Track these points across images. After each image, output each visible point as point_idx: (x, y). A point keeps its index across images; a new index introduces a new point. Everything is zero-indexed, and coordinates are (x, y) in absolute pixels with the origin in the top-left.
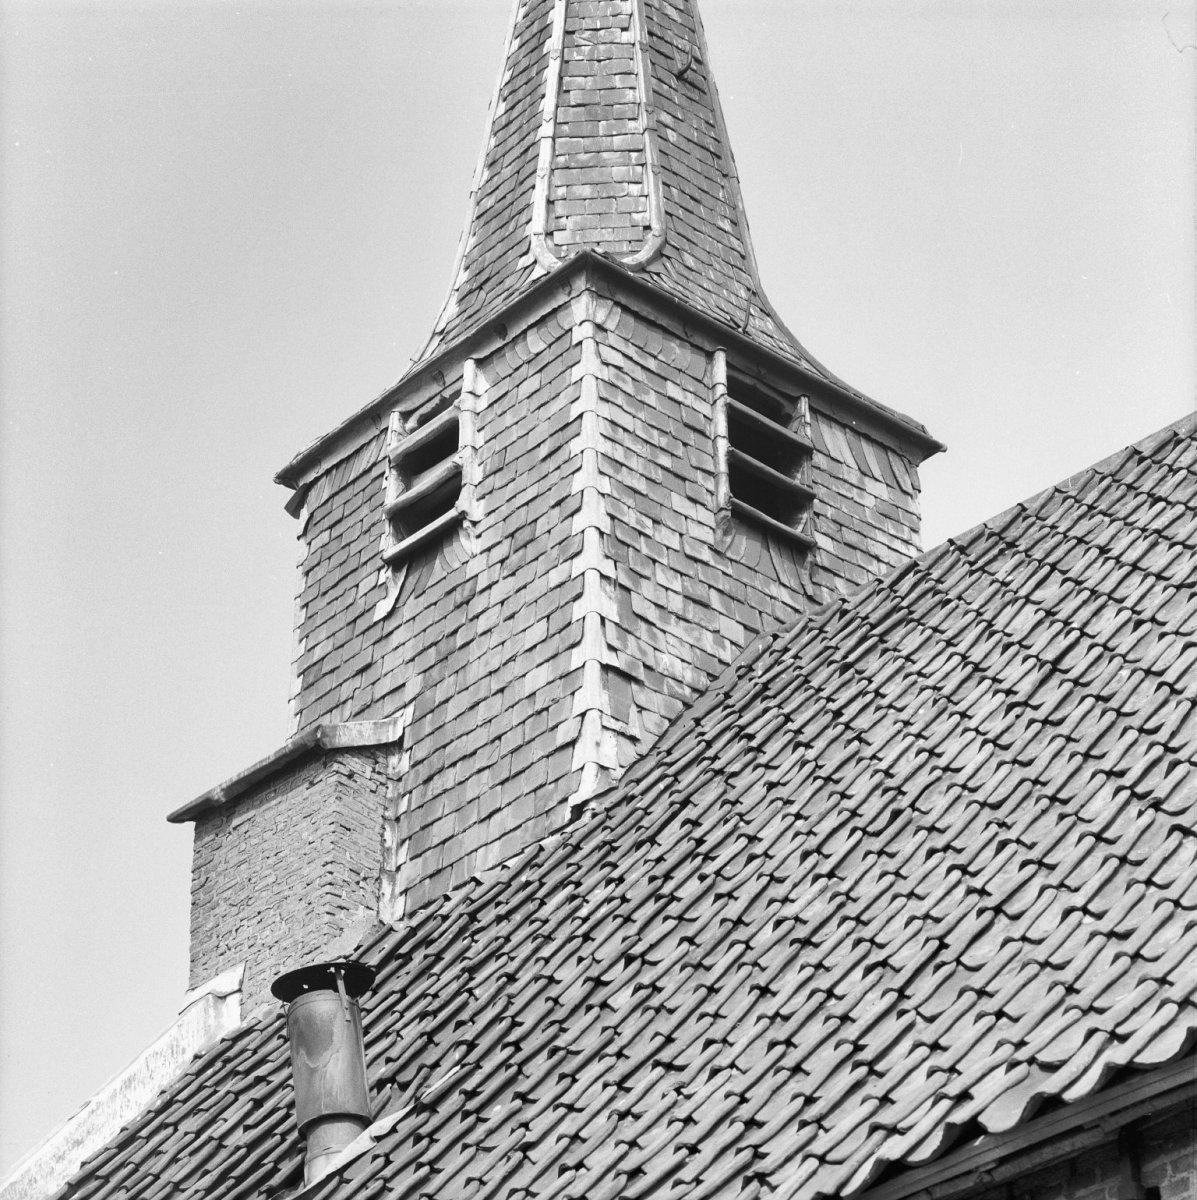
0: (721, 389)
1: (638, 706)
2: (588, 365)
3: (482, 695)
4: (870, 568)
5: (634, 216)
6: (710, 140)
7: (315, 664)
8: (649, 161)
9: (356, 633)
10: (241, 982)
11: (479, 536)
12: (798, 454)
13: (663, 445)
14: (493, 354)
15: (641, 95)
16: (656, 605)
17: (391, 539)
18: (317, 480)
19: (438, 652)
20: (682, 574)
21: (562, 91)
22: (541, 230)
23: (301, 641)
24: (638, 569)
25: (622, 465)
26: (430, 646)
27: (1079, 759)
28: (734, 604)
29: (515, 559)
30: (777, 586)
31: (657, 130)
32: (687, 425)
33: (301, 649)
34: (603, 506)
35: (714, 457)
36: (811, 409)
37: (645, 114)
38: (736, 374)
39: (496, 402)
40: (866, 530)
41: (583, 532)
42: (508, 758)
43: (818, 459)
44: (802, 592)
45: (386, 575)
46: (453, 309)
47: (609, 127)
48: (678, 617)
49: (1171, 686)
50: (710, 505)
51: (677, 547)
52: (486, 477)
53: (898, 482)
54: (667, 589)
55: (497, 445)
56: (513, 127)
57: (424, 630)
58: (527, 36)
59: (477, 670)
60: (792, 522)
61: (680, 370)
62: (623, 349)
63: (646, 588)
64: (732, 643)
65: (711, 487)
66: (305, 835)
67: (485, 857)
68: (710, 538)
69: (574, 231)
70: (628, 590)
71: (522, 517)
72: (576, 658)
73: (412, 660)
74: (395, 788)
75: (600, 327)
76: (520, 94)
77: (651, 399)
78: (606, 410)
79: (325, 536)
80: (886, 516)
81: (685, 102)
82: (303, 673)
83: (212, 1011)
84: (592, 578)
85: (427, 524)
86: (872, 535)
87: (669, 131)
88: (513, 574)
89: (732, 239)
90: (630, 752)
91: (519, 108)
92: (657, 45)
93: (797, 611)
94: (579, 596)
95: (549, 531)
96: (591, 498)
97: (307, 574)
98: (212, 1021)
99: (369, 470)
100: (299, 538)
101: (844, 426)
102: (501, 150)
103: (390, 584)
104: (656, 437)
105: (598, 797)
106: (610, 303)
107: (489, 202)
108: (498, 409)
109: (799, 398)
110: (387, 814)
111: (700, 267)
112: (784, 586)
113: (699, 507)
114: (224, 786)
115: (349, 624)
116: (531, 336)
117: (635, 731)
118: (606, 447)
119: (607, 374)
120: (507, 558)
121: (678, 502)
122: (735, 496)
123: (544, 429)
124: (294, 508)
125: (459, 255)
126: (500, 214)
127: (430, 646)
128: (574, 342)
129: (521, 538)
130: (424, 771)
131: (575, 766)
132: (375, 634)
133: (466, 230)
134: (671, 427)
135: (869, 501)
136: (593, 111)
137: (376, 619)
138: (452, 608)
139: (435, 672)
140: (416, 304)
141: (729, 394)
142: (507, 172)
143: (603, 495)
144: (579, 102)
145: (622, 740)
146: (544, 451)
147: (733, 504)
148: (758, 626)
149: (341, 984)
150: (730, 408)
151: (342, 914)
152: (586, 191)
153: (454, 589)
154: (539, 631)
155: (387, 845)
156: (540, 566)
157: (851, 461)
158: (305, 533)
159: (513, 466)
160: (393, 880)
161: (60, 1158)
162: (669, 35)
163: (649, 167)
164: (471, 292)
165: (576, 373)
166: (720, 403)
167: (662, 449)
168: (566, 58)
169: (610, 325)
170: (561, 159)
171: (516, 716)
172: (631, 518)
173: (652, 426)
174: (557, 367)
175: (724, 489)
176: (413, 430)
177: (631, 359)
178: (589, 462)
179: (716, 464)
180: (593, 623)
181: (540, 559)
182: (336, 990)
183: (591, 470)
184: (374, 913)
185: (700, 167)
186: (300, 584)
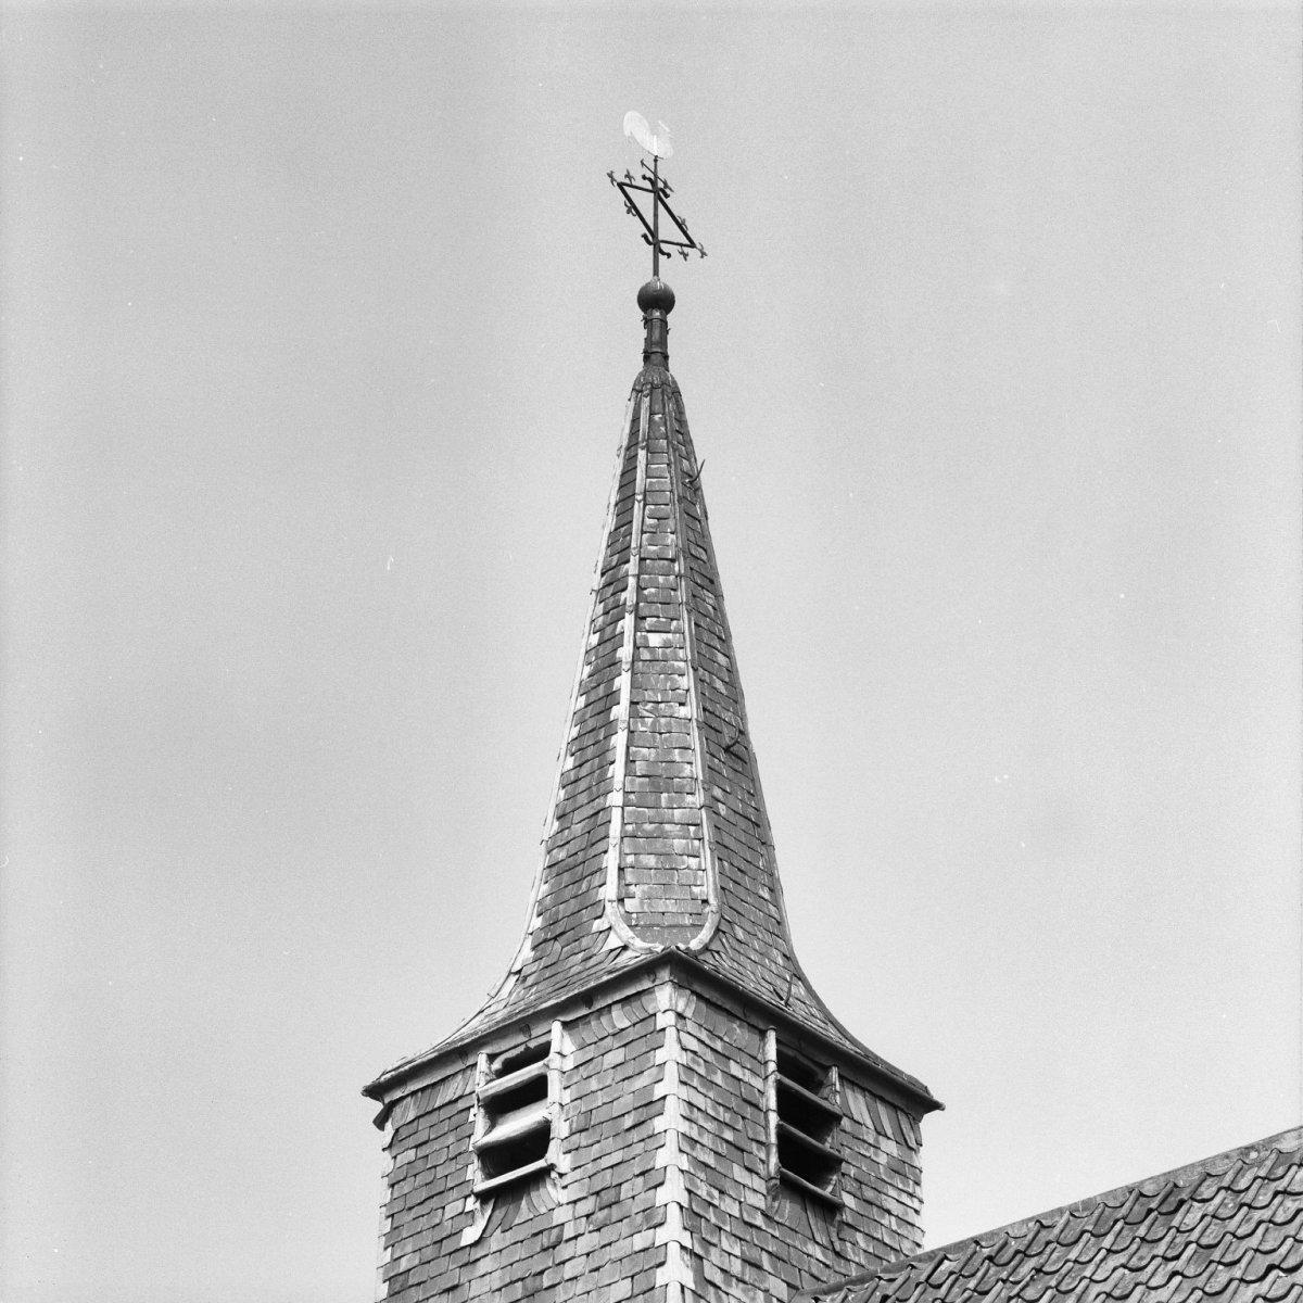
0: (772, 1066)
2: (669, 1053)
4: (883, 1222)
5: (693, 888)
6: (751, 810)
7: (401, 1274)
8: (706, 838)
11: (565, 1187)
12: (826, 1121)
13: (727, 1121)
14: (577, 1019)
15: (697, 770)
16: (722, 1270)
17: (479, 1175)
18: (402, 1098)
19: (525, 1288)
20: (741, 1239)
22: (614, 898)
23: (386, 1249)
24: (708, 1238)
25: (697, 1142)
28: (779, 1264)
29: (600, 1215)
31: (710, 806)
32: (745, 1100)
33: (387, 1256)
35: (766, 1127)
36: (841, 1077)
37: (702, 790)
39: (581, 1065)
40: (879, 1185)
41: (666, 1205)
43: (845, 1122)
44: (831, 1248)
45: (471, 1204)
46: (527, 953)
47: (670, 800)
48: (738, 1279)
50: (763, 1173)
51: (737, 1215)
52: (572, 1134)
53: (905, 1139)
54: (730, 1254)
57: (512, 1265)
60: (823, 1183)
61: (740, 1049)
62: (698, 1035)
65: (763, 1156)
68: (760, 1202)
70: (701, 1258)
71: (607, 1178)
73: (500, 1289)
75: (680, 1016)
77: (718, 1079)
78: (684, 1092)
80: (895, 1172)
82: (389, 1279)
84: (674, 1249)
86: (885, 1191)
87: (720, 805)
89: (771, 907)
92: (709, 726)
93: (827, 1266)
94: (662, 1264)
95: (633, 1197)
96: (672, 1174)
97: (392, 1186)
99: (456, 1100)
100: (384, 1150)
101: (863, 1090)
103: (478, 1214)
106: (688, 992)
107: (561, 854)
109: (830, 1067)
112: (817, 1243)
113: (754, 1176)
115: (435, 1243)
116: (616, 1012)
118: (684, 1127)
119: (685, 1058)
120: (593, 1214)
121: (739, 1173)
122: (783, 1167)
123: (627, 1101)
124: (380, 1122)
125: (532, 901)
129: (607, 1199)
132: (463, 1258)
133: (538, 877)
134: (734, 1103)
135: (883, 1159)
136: (657, 782)
137: (463, 1244)
138: (538, 1249)
141: (778, 1071)
142: (578, 829)
143: (682, 1171)
144: (644, 773)
146: (628, 1121)
147: (781, 1173)
148: (798, 1284)
150: (779, 1084)
152: (651, 861)
153: (541, 1232)
156: (624, 1228)
157: (869, 1123)
158: (390, 1146)
163: (706, 843)
164: (545, 941)
166: (772, 1079)
167: (726, 1124)
168: (632, 729)
169: (689, 1014)
170: (629, 828)
173: (720, 1104)
174: (640, 1047)
175: (774, 1159)
178: (671, 1140)
179: (767, 1135)
181: (625, 1221)
183: (673, 1149)
185: (744, 840)
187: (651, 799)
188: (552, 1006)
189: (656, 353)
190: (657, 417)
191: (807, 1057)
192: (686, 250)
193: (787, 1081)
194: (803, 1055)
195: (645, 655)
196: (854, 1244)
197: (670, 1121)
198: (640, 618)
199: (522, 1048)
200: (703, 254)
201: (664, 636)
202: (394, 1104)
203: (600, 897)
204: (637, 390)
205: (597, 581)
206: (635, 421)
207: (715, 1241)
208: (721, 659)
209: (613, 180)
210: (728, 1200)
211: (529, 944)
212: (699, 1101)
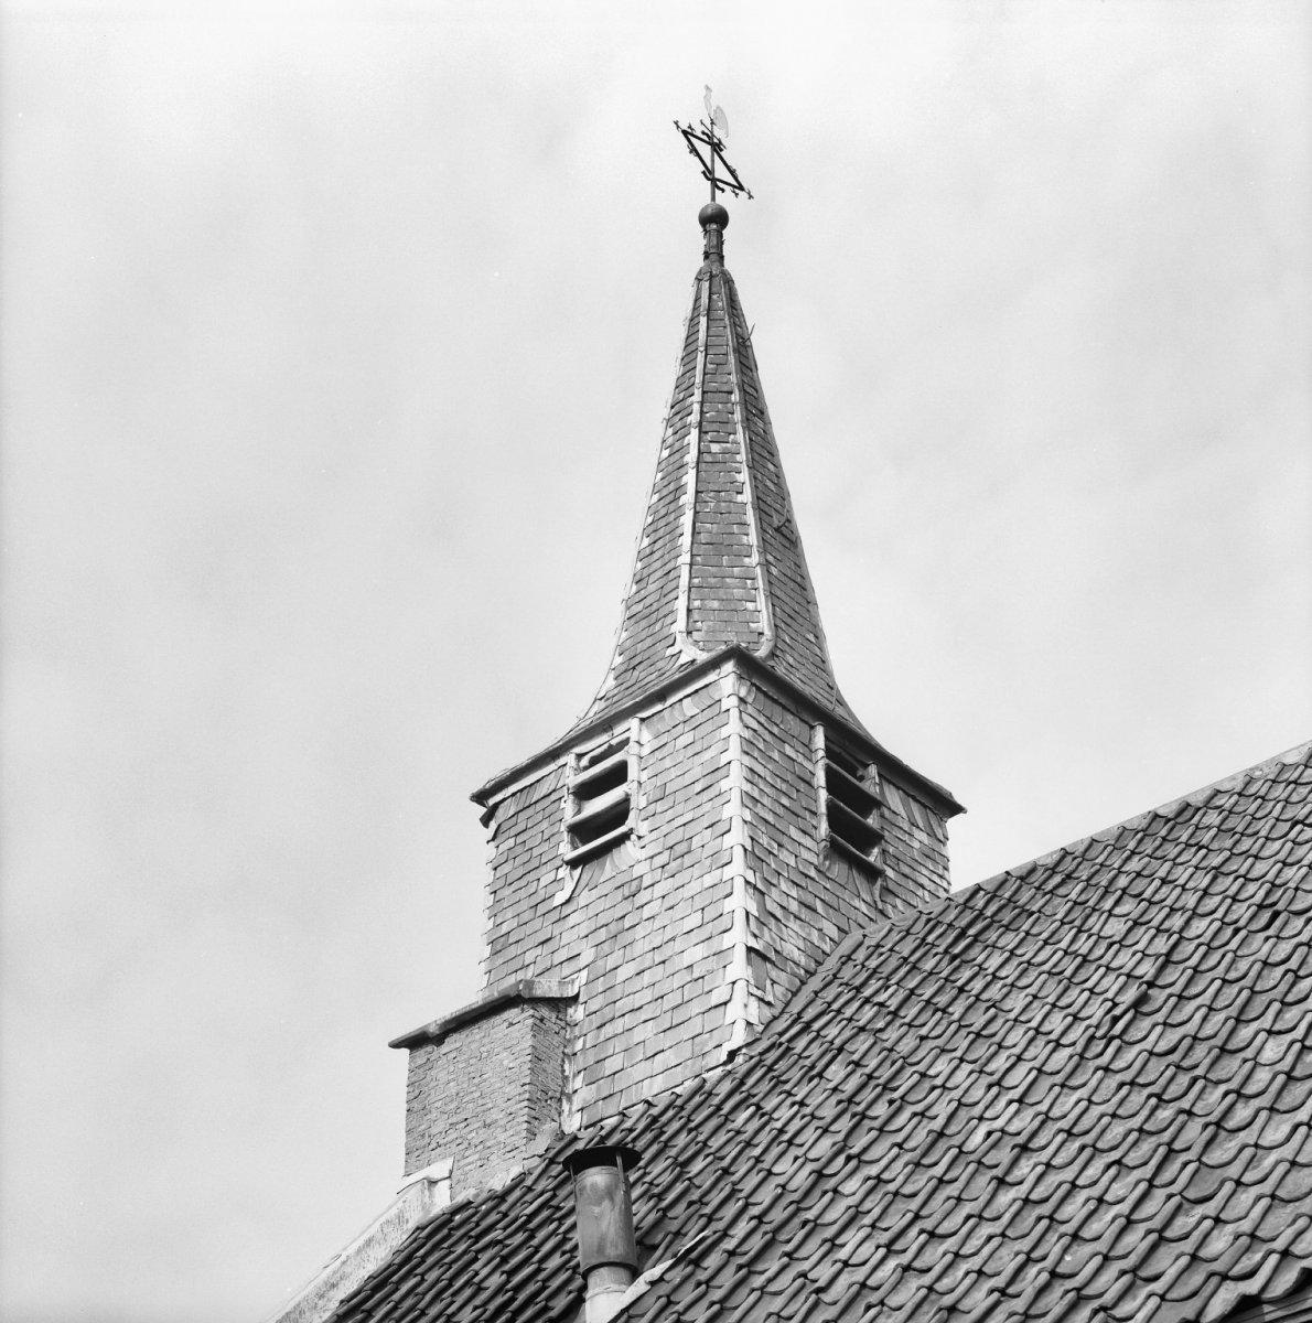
0: (821, 753)
1: (772, 980)
3: (647, 965)
5: (751, 625)
9: (538, 915)
10: (451, 1172)
12: (870, 804)
20: (798, 885)
21: (694, 532)
25: (757, 801)
26: (602, 927)
27: (879, 1089)
28: (831, 911)
30: (860, 896)
31: (766, 565)
33: (490, 924)
34: (747, 830)
38: (832, 746)
42: (669, 1014)
45: (564, 872)
46: (611, 683)
48: (796, 917)
49: (1295, 972)
55: (659, 781)
56: (656, 556)
58: (665, 492)
59: (639, 948)
63: (774, 893)
64: (830, 939)
66: (505, 1062)
67: (651, 1087)
69: (707, 632)
70: (763, 894)
71: (678, 835)
72: (726, 941)
74: (572, 1032)
76: (661, 533)
77: (776, 755)
78: (747, 760)
79: (511, 842)
81: (781, 548)
83: (426, 1192)
85: (599, 835)
88: (673, 876)
90: (768, 1013)
91: (660, 543)
93: (871, 919)
97: (495, 869)
98: (427, 1200)
99: (550, 794)
100: (488, 842)
101: (898, 788)
102: (646, 572)
104: (779, 784)
105: (748, 1045)
108: (658, 755)
110: (566, 1051)
111: (798, 666)
114: (438, 1022)
117: (769, 998)
118: (747, 787)
119: (747, 734)
121: (794, 832)
123: (697, 772)
124: (486, 821)
126: (645, 614)
127: (602, 927)
128: (723, 709)
129: (678, 853)
130: (596, 1020)
131: (728, 1020)
132: (555, 916)
134: (789, 777)
135: (916, 845)
139: (606, 947)
140: (580, 680)
142: (652, 587)
143: (746, 822)
145: (762, 1004)
146: (698, 787)
148: (846, 929)
149: (619, 1160)
151: (536, 1123)
152: (716, 604)
154: (695, 920)
155: (566, 1074)
156: (696, 871)
157: (904, 815)
158: (493, 839)
159: (671, 798)
160: (569, 1099)
161: (322, 1297)
162: (769, 500)
165: (724, 732)
169: (750, 700)
170: (696, 581)
171: (677, 982)
172: (764, 840)
174: (708, 727)
176: (586, 768)
177: (762, 725)
178: (735, 797)
180: (740, 917)
182: (616, 1165)
184: (556, 1125)
186: (488, 876)
187: (714, 560)
188: (630, 706)
189: (714, 253)
190: (715, 297)
191: (851, 755)
192: (737, 191)
193: (835, 766)
194: (848, 753)
195: (708, 458)
196: (895, 907)
197: (734, 782)
198: (702, 432)
199: (606, 746)
200: (751, 197)
201: (724, 445)
202: (496, 806)
203: (672, 631)
204: (699, 280)
205: (666, 412)
206: (697, 299)
207: (775, 881)
208: (771, 467)
209: (678, 127)
210: (785, 852)
211: (612, 676)
212: (759, 769)
